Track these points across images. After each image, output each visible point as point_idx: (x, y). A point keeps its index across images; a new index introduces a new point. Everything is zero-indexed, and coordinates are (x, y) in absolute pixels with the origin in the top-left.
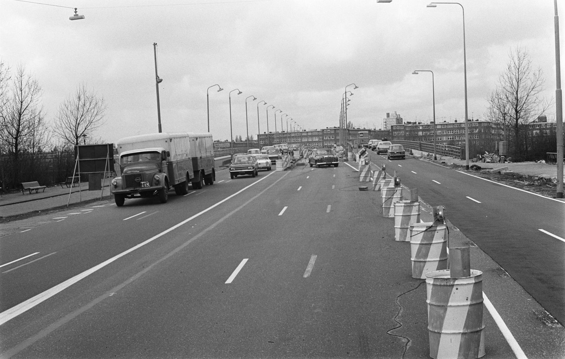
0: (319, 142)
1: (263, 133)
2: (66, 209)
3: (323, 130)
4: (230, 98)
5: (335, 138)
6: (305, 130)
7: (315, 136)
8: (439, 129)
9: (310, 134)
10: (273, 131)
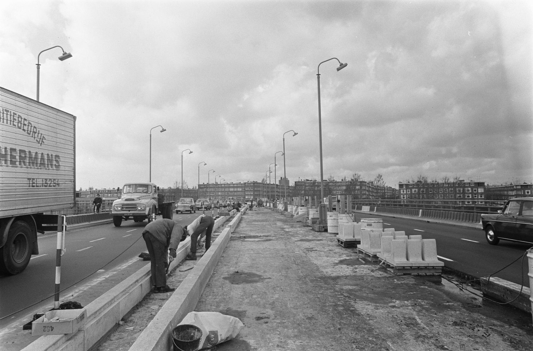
0: (242, 191)
1: (202, 184)
2: (382, 305)
3: (245, 183)
4: (151, 136)
5: (254, 189)
6: (232, 183)
7: (239, 187)
8: (307, 186)
9: (223, 186)
10: (211, 183)
